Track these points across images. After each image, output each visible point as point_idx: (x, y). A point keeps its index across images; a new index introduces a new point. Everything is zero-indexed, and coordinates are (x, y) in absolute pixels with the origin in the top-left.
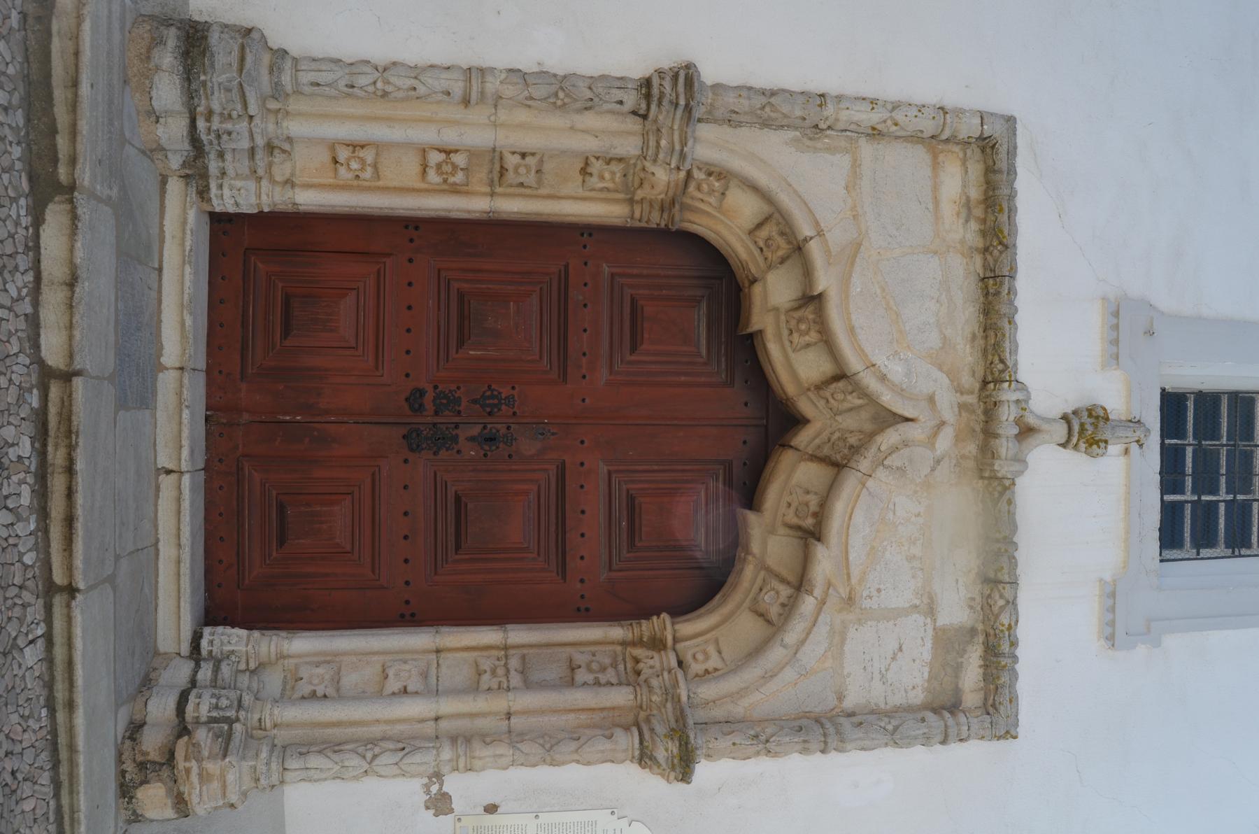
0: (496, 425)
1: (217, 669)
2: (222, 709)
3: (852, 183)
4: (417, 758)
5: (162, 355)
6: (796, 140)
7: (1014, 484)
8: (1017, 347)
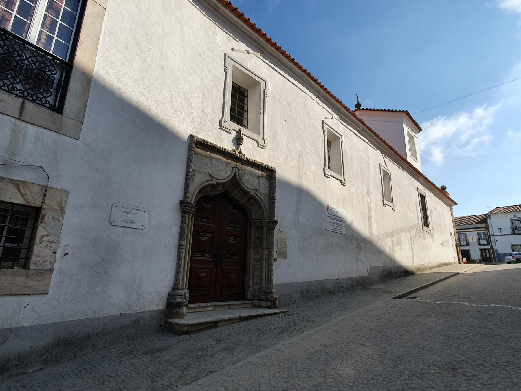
1: (256, 296)
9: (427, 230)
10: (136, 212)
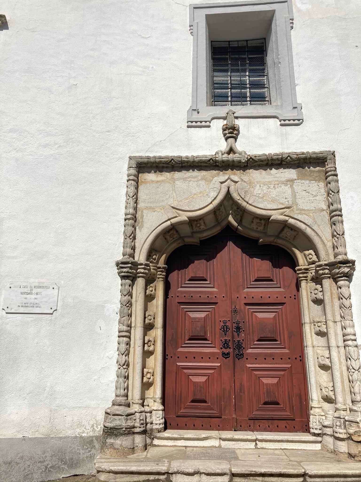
0: (233, 327)
2: (341, 425)
3: (152, 209)
4: (352, 354)
5: (215, 446)
6: (139, 228)
7: (249, 155)
8: (205, 155)
9: (282, 321)
10: (39, 290)
